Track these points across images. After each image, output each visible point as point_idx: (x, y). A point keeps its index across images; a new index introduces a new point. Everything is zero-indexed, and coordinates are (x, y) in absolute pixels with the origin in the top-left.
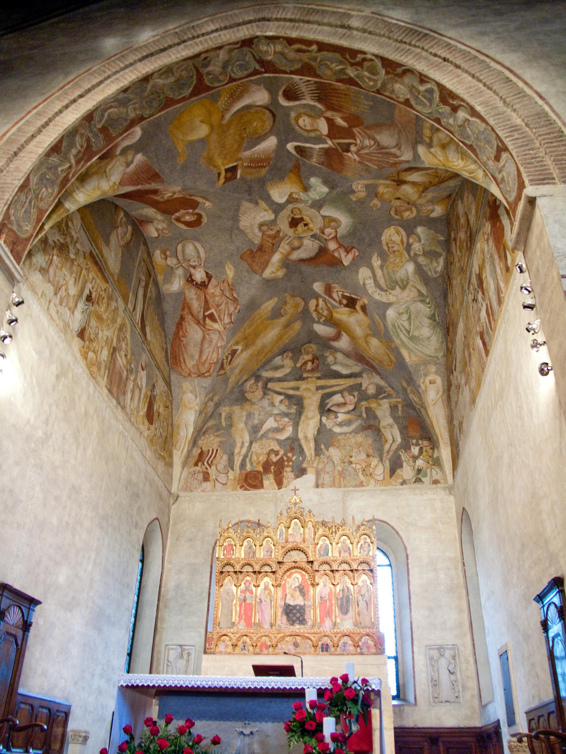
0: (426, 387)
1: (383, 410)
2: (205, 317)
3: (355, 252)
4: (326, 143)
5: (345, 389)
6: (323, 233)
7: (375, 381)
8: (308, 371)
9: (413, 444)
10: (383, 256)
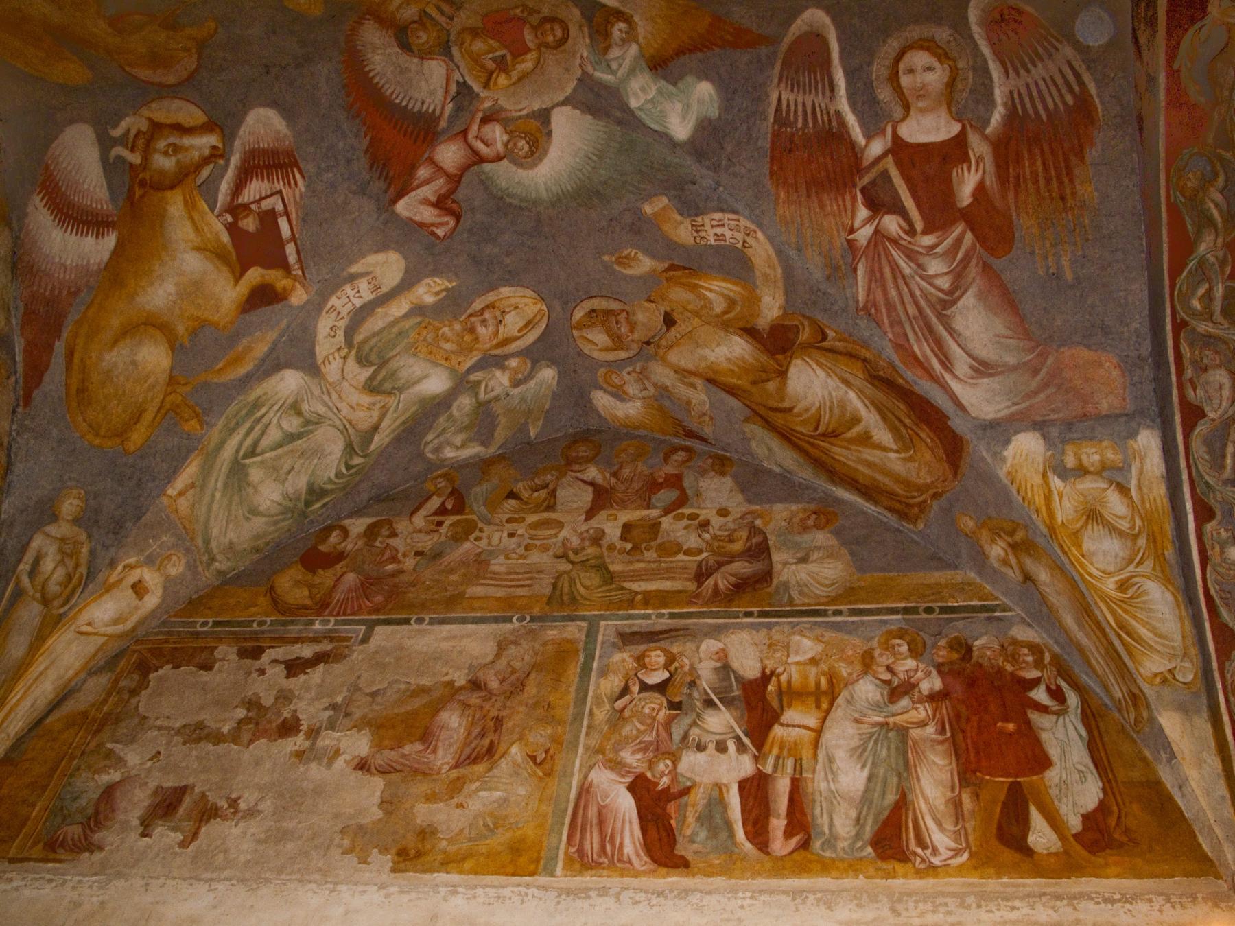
0: (120, 581)
4: (869, 138)
6: (485, 120)
10: (452, 304)
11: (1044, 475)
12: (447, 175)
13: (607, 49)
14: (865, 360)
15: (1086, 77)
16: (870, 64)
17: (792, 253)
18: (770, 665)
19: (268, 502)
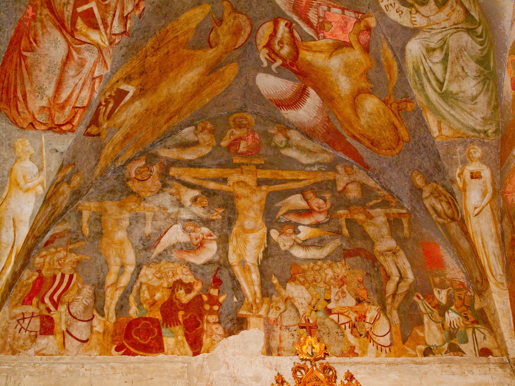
0: (464, 183)
1: (377, 225)
2: (75, 15)
5: (310, 188)
9: (436, 286)
19: (474, 88)
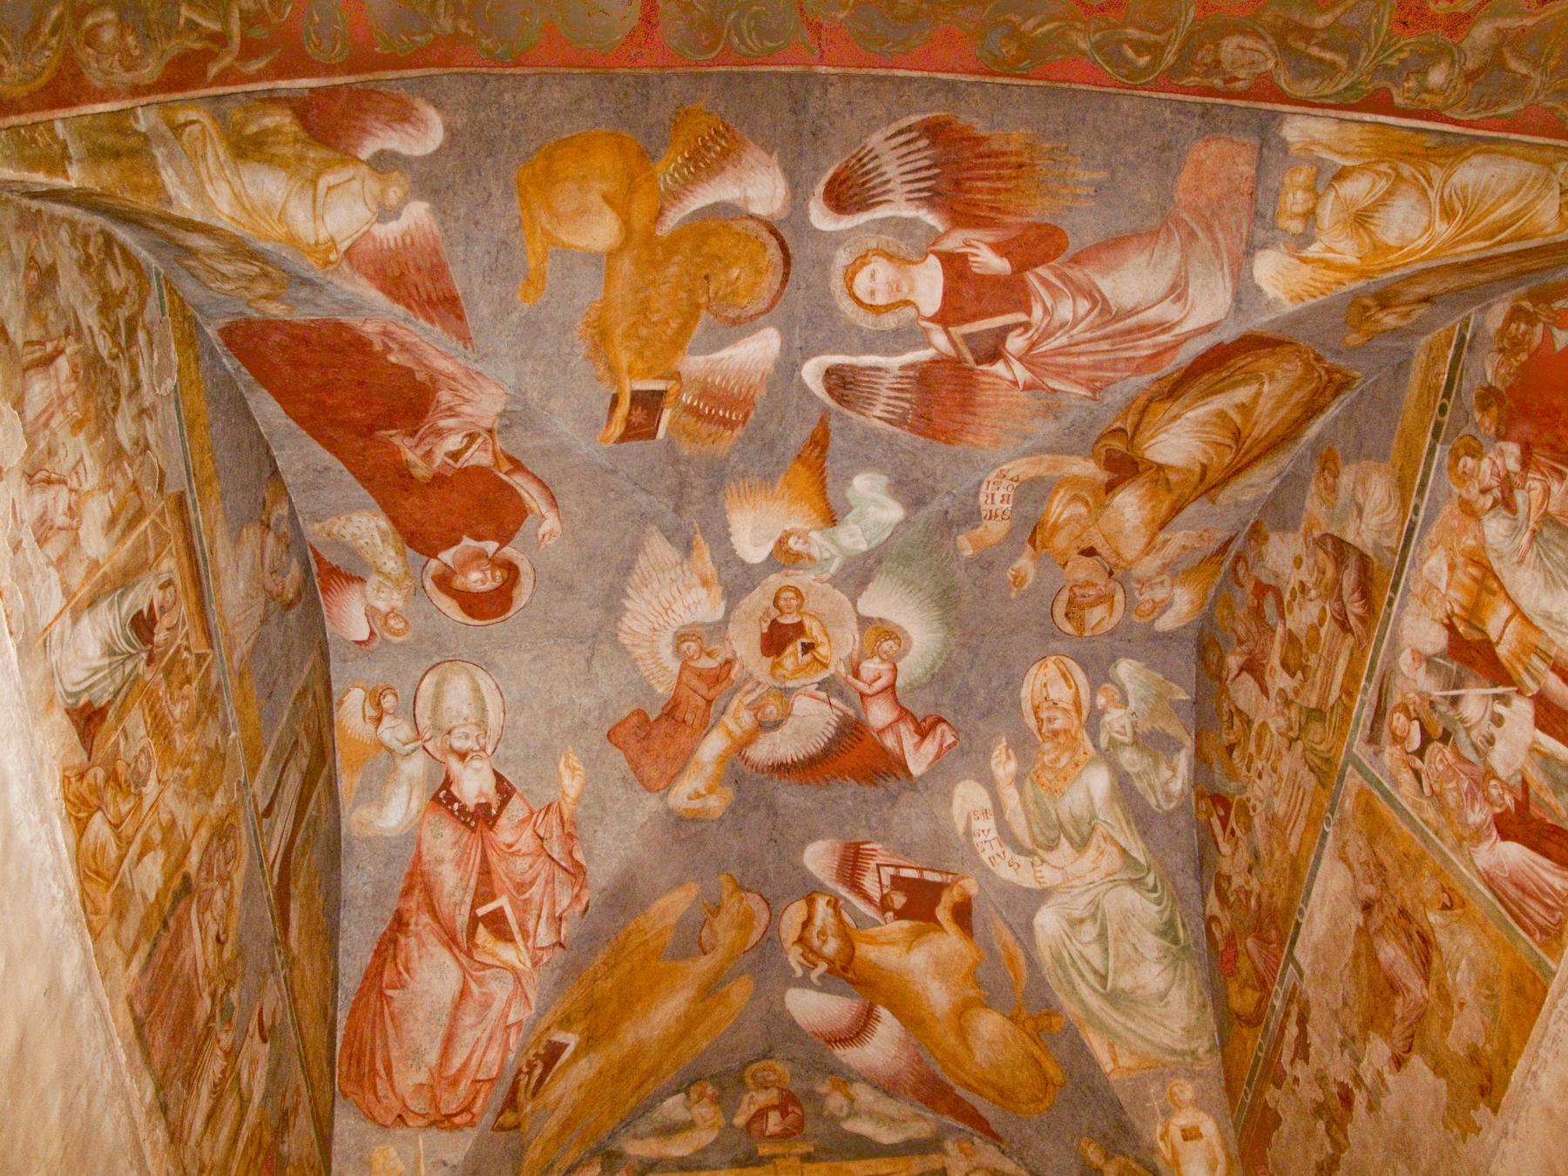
0: (1174, 1153)
2: (474, 921)
3: (945, 735)
4: (929, 344)
7: (986, 1162)
8: (773, 1136)
10: (1023, 746)
11: (1304, 260)
12: (897, 721)
13: (811, 558)
14: (1150, 401)
15: (904, 123)
16: (860, 330)
17: (1027, 444)
18: (1440, 614)
